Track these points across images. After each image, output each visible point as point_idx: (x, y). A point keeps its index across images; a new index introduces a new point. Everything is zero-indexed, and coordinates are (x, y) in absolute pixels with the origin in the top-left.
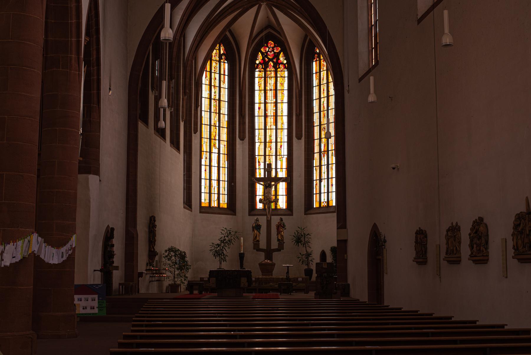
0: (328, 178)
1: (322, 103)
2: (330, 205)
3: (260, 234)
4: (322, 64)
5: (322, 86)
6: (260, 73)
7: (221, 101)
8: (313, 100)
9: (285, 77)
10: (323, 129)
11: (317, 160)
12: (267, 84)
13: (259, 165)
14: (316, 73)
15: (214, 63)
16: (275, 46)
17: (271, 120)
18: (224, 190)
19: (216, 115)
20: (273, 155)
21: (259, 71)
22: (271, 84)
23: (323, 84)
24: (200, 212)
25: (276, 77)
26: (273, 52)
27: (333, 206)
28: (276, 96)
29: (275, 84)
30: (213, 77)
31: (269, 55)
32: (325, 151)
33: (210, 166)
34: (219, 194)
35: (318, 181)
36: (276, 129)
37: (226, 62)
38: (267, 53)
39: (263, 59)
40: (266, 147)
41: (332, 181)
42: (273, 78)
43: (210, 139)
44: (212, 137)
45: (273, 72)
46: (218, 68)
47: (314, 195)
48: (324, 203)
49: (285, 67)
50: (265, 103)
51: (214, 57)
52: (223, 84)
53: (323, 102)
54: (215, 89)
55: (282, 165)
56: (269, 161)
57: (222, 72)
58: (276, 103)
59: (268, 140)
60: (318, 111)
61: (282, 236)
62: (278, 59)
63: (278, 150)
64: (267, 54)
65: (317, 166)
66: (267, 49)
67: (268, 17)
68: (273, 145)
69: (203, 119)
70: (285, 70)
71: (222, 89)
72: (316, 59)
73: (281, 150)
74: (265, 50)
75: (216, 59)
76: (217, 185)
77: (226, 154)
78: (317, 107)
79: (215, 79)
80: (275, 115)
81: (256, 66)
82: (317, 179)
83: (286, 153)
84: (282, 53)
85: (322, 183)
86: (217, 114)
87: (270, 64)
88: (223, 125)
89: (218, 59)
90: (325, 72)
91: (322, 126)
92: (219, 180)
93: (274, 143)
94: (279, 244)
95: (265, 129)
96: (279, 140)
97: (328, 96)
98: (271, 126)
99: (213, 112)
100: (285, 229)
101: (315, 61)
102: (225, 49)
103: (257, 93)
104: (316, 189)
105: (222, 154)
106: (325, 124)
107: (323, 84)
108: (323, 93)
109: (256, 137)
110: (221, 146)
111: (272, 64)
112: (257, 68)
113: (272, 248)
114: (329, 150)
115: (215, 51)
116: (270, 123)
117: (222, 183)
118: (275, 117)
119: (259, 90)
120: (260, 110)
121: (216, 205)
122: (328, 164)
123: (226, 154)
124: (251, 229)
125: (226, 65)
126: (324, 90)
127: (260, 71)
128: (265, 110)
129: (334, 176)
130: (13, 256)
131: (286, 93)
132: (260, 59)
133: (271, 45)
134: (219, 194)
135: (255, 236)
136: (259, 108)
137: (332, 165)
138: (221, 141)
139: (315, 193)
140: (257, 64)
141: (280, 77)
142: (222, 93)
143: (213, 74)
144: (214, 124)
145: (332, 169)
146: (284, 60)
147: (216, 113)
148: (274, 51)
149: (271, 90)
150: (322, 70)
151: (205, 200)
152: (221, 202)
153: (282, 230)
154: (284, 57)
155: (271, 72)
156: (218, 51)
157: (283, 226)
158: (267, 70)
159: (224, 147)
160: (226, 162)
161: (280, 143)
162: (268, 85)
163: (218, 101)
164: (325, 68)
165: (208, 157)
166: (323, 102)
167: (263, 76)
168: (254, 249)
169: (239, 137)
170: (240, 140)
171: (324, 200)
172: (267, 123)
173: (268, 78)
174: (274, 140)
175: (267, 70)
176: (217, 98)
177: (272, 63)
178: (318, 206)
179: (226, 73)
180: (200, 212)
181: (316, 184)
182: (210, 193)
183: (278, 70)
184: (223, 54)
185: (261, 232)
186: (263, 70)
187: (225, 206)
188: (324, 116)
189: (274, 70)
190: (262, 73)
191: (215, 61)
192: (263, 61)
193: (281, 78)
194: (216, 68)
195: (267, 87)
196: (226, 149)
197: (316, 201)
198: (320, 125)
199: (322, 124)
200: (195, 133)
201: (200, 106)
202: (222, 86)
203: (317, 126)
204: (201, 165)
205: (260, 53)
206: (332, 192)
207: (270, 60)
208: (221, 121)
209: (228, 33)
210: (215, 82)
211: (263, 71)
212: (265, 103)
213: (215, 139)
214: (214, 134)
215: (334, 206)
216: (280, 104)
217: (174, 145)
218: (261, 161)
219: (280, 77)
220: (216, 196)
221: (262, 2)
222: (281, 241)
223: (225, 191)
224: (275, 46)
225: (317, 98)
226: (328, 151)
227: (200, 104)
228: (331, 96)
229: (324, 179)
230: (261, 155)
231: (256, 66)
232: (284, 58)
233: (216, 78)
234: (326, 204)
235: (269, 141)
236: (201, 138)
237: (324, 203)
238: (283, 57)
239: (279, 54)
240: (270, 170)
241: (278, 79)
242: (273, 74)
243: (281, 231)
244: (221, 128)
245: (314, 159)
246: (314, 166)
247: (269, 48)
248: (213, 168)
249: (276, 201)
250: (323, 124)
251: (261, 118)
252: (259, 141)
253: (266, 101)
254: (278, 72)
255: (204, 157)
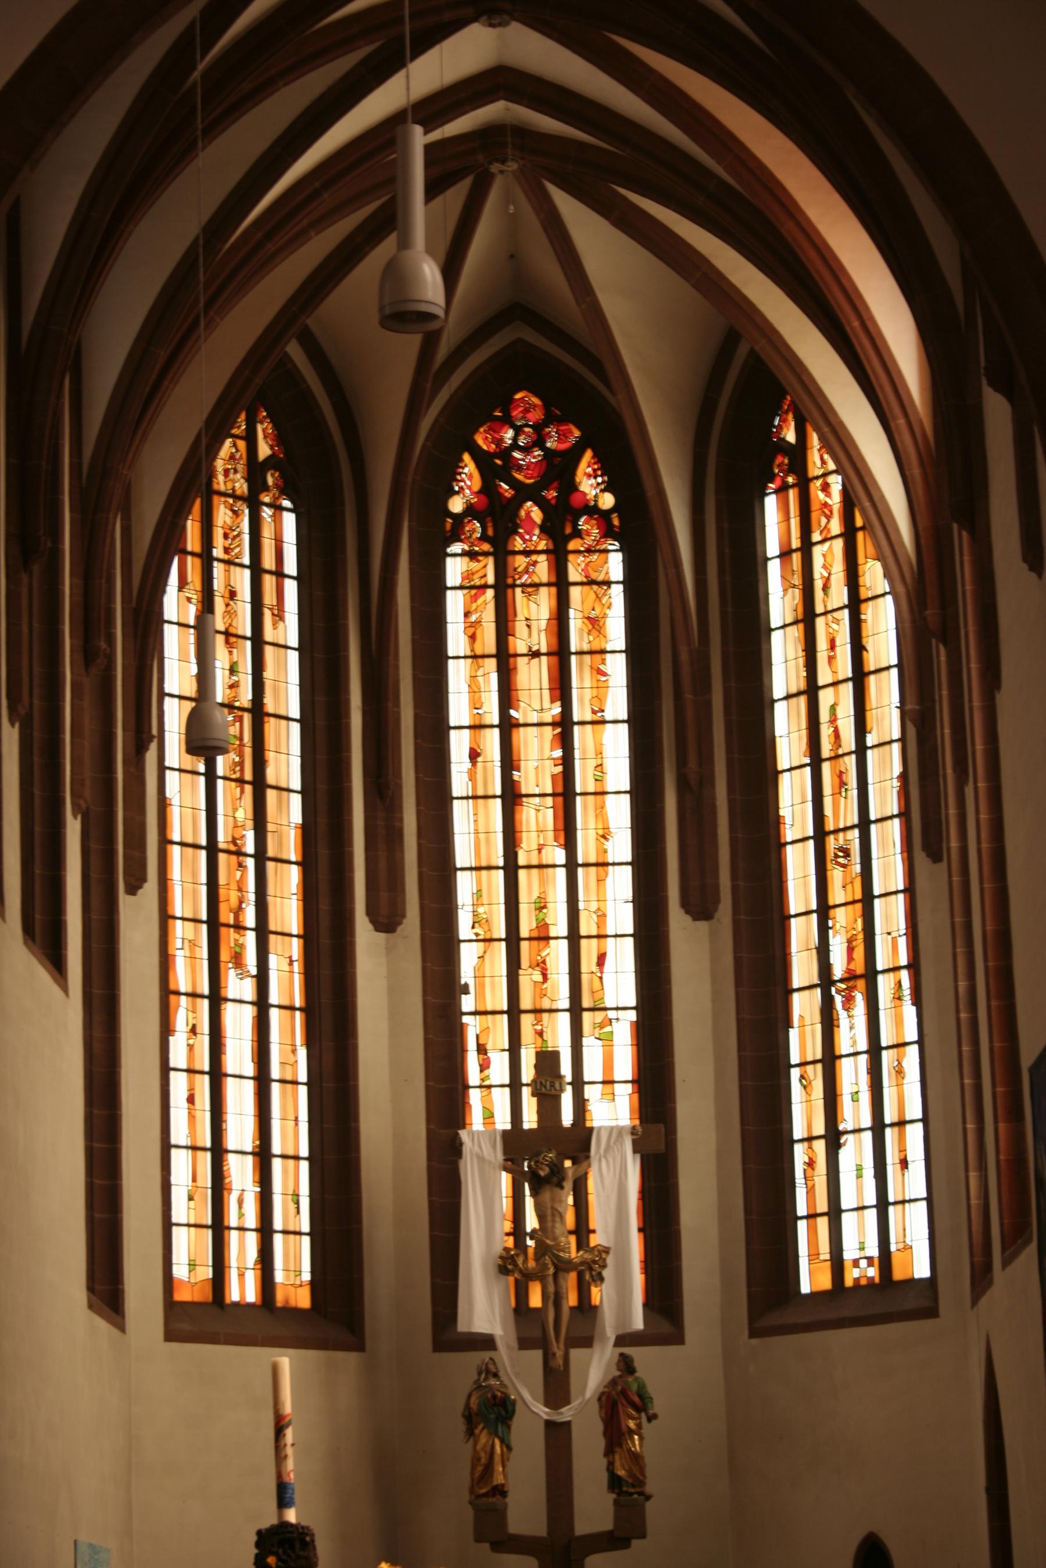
0: (878, 1128)
1: (824, 716)
2: (898, 1275)
3: (509, 1448)
4: (815, 506)
5: (820, 622)
6: (474, 566)
7: (266, 719)
8: (773, 701)
9: (608, 583)
10: (836, 856)
11: (808, 1029)
12: (510, 624)
13: (484, 1066)
14: (785, 554)
15: (222, 507)
16: (549, 419)
17: (540, 814)
18: (292, 1207)
19: (242, 792)
20: (557, 1010)
21: (464, 554)
22: (534, 624)
23: (825, 613)
24: (170, 1336)
25: (561, 584)
26: (538, 453)
27: (912, 1281)
28: (562, 689)
29: (554, 622)
30: (218, 584)
31: (520, 468)
32: (851, 977)
33: (217, 1075)
34: (265, 1230)
35: (820, 1146)
36: (571, 866)
37: (287, 503)
38: (505, 453)
39: (488, 489)
40: (519, 967)
41: (902, 1139)
42: (544, 591)
43: (214, 924)
44: (226, 916)
45: (542, 558)
46: (246, 538)
47: (802, 1226)
48: (863, 1263)
49: (608, 532)
50: (507, 726)
51: (221, 478)
52: (275, 625)
53: (833, 708)
54: (231, 653)
55: (608, 1063)
56: (539, 1040)
57: (268, 562)
58: (564, 726)
59: (526, 928)
60: (807, 760)
61: (636, 1459)
62: (570, 487)
63: (585, 978)
64: (511, 462)
65: (810, 1058)
66: (509, 435)
67: (512, 256)
68: (558, 953)
69: (175, 814)
70: (611, 548)
71: (269, 651)
72: (778, 481)
73: (601, 978)
74: (499, 441)
75: (233, 489)
76: (257, 1178)
77: (299, 1009)
78: (800, 738)
79: (233, 595)
80: (560, 790)
81: (448, 527)
82: (815, 1133)
83: (630, 998)
84: (588, 455)
85: (847, 1157)
86: (248, 788)
87: (528, 514)
88: (280, 845)
89: (241, 486)
90: (838, 545)
91: (831, 843)
92: (263, 1155)
93: (564, 944)
94: (616, 1502)
95: (511, 868)
96: (587, 926)
97: (859, 677)
98: (540, 850)
99: (224, 778)
100: (649, 1420)
101: (777, 492)
102: (280, 438)
103: (457, 674)
104: (811, 1191)
105: (280, 1007)
106: (845, 829)
107: (825, 613)
108: (831, 659)
109: (460, 912)
110: (273, 961)
111: (537, 515)
112: (455, 536)
113: (582, 1527)
114: (879, 968)
115: (228, 442)
116: (534, 835)
117: (285, 1171)
118: (560, 799)
119: (469, 653)
120: (479, 765)
121: (251, 1296)
122: (875, 1050)
123: (299, 1009)
124: (461, 1425)
125: (289, 521)
126: (832, 646)
127: (471, 555)
128: (509, 762)
129: (914, 1109)
130: (482, 959)
131: (617, 667)
132: (469, 488)
133: (527, 411)
134: (265, 1230)
135: (483, 1461)
136: (474, 755)
137: (901, 1049)
138: (272, 938)
139: (802, 1209)
140: (456, 514)
141: (582, 584)
142: (269, 674)
143: (218, 569)
144: (234, 841)
145: (899, 1072)
146: (602, 491)
147: (241, 781)
148: (542, 447)
149: (535, 654)
150: (816, 537)
151: (192, 1265)
152: (279, 1277)
153: (632, 1424)
154: (602, 476)
155: (534, 557)
156: (242, 444)
157: (636, 1399)
158: (510, 548)
159: (287, 968)
160: (302, 1053)
161: (594, 941)
162: (520, 627)
163: (247, 718)
164: (836, 526)
165: (205, 1027)
166: (833, 708)
167: (491, 579)
168: (479, 1539)
169: (372, 912)
170: (377, 929)
171: (862, 1249)
172: (518, 835)
173: (518, 590)
174: (560, 927)
175: (510, 548)
176: (246, 696)
177: (535, 508)
178: (825, 1282)
179: (291, 566)
180: (170, 1336)
181: (811, 1164)
182: (219, 1228)
183: (572, 545)
184: (271, 462)
185: (514, 1438)
186: (486, 547)
187: (303, 1300)
188: (842, 784)
189: (551, 547)
190: (482, 564)
191: (231, 501)
192: (484, 499)
193: (586, 588)
194: (235, 537)
195: (511, 638)
196: (298, 980)
197: (813, 1255)
198: (820, 835)
199: (830, 826)
200: (133, 889)
201: (155, 741)
202: (269, 634)
203: (805, 839)
204: (165, 1069)
205: (466, 457)
206: (903, 1202)
207: (524, 493)
208: (270, 827)
209: (294, 350)
210: (230, 613)
211: (486, 554)
212: (507, 726)
213: (239, 927)
214: (234, 896)
215: (921, 1280)
216: (589, 727)
217: (33, 940)
218: (494, 1043)
219: (582, 584)
220: (252, 1240)
221: (497, 161)
222: (633, 1486)
223: (298, 1212)
224: (549, 419)
225: (793, 690)
226: (871, 974)
227: (155, 732)
228: (878, 675)
229: (854, 1131)
230: (494, 1013)
231: (448, 527)
232: (600, 480)
233: (238, 589)
234: (872, 1272)
235: (535, 934)
236: (165, 917)
237: (863, 1263)
238: (595, 477)
239: (572, 457)
240: (552, 1086)
241: (575, 593)
242: (542, 570)
243: (631, 1432)
244: (270, 866)
245: (788, 1024)
246: (795, 1059)
247: (518, 431)
248: (231, 1086)
249: (595, 1262)
250: (836, 831)
251: (486, 807)
252: (477, 934)
253: (513, 712)
254: (571, 557)
255: (181, 1021)
